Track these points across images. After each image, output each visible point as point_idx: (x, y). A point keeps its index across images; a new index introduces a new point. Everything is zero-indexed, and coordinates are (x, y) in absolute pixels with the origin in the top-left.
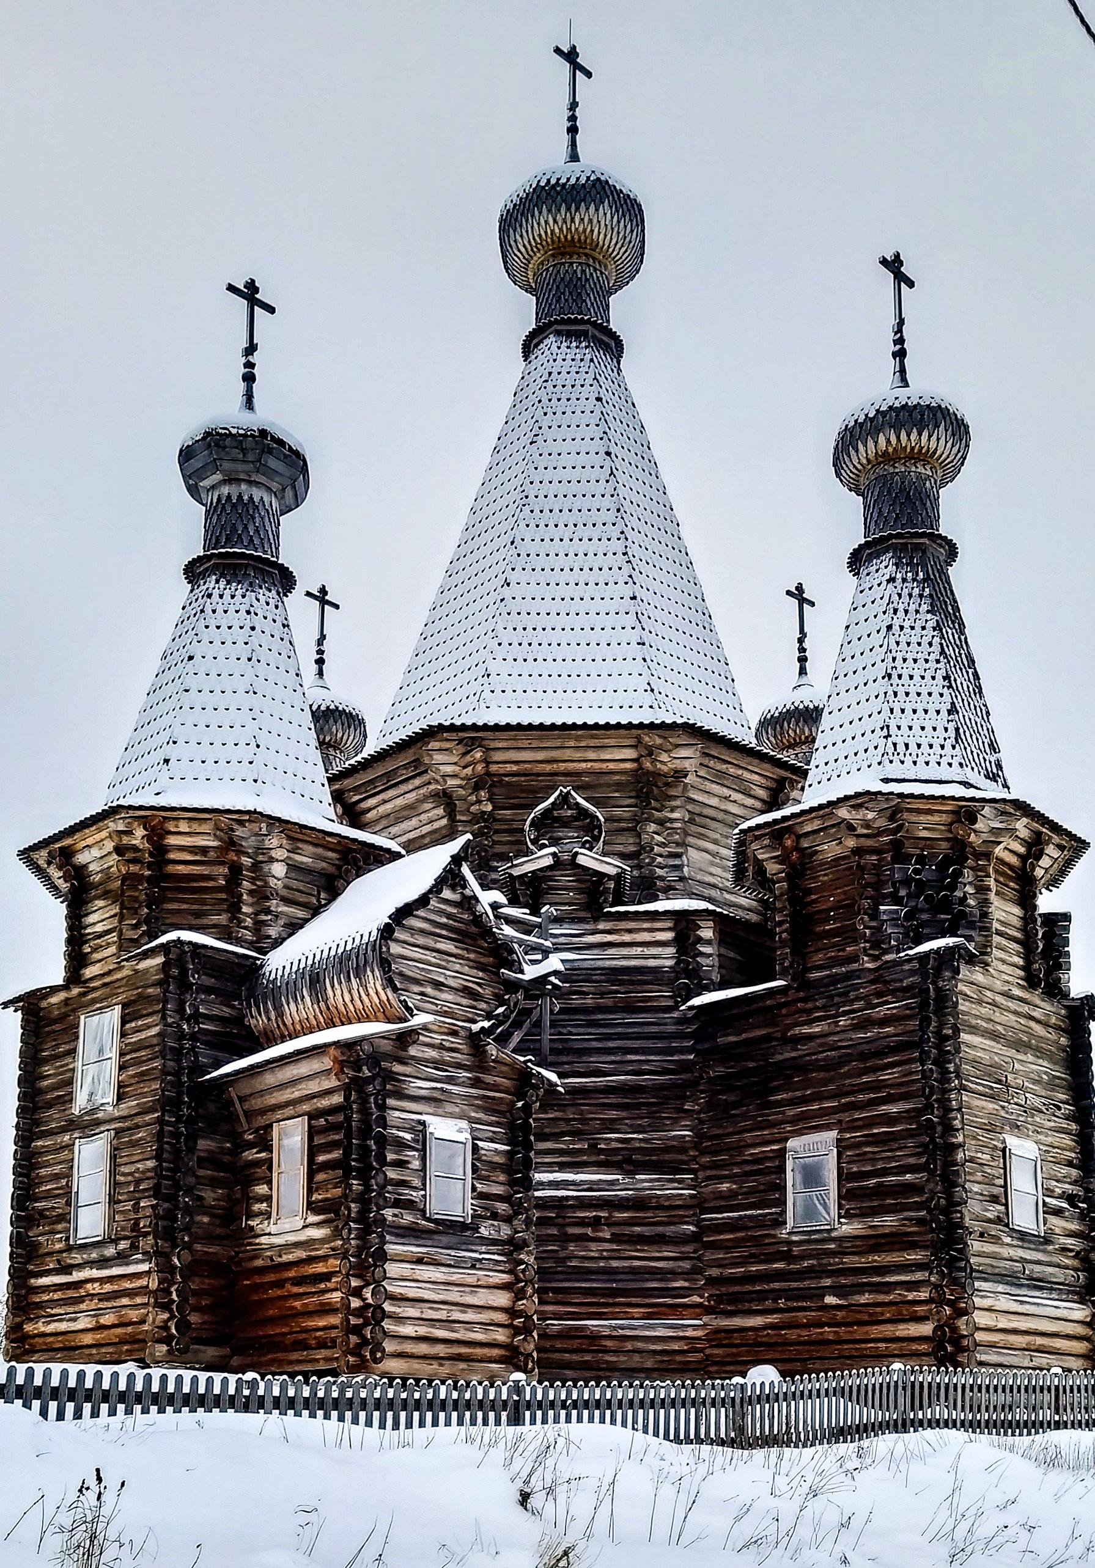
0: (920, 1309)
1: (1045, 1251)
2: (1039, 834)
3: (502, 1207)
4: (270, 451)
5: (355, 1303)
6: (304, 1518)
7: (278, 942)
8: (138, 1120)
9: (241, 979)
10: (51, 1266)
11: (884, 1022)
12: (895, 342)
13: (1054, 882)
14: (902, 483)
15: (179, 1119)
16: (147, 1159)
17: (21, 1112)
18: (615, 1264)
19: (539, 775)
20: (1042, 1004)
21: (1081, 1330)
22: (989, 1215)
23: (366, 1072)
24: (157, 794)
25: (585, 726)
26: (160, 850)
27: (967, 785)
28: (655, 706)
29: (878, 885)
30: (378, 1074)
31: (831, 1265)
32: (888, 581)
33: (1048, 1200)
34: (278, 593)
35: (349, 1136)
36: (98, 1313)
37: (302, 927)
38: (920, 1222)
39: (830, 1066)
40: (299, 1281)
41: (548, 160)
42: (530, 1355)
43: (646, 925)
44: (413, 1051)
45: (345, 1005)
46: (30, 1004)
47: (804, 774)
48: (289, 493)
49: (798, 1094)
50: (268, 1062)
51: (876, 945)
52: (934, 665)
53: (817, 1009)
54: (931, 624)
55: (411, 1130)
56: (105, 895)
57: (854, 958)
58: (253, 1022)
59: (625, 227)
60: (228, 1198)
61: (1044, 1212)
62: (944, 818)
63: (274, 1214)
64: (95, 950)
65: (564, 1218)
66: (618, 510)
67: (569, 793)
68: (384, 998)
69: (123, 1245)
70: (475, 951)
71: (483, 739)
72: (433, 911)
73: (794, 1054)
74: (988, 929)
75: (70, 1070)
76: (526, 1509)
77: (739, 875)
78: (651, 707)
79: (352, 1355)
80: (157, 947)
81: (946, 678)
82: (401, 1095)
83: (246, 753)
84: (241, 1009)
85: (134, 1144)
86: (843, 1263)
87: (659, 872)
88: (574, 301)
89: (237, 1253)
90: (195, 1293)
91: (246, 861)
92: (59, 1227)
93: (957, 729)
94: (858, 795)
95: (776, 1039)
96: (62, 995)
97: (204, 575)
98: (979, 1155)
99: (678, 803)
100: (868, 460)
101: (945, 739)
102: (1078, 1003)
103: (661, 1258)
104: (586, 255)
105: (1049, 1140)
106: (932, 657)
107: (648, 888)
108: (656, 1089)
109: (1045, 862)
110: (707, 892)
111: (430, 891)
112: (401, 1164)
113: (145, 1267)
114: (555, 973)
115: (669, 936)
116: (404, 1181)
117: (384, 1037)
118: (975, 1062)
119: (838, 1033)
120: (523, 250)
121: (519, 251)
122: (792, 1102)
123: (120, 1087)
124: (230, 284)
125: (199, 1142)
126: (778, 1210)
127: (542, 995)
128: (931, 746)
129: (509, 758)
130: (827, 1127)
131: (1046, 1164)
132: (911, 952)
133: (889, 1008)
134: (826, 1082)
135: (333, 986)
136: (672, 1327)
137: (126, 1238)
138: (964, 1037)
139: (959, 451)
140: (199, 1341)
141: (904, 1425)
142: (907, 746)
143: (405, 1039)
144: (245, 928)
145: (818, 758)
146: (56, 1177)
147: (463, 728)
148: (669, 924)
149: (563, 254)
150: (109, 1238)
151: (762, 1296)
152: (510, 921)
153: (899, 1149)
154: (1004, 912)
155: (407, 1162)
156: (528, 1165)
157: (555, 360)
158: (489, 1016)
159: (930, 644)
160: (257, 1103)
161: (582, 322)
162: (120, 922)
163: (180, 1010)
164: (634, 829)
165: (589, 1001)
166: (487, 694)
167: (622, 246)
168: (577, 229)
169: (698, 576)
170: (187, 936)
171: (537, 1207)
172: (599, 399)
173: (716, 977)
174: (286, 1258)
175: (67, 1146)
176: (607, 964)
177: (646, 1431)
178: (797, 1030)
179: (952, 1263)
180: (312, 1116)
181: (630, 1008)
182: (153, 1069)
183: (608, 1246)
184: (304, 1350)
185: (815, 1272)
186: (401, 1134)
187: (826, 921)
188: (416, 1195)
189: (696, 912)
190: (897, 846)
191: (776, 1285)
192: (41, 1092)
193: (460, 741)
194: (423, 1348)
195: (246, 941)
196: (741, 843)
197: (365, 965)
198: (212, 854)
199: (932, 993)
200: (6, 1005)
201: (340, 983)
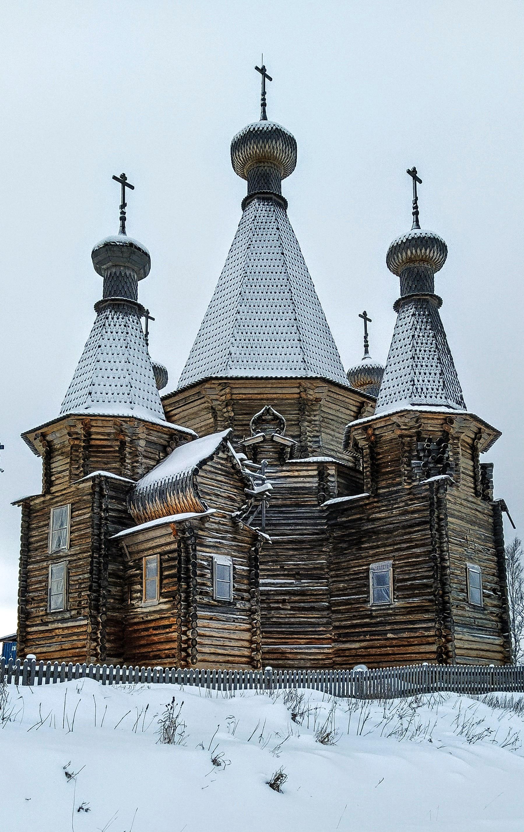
0: (430, 640)
1: (483, 614)
2: (480, 429)
3: (246, 595)
5: (184, 638)
6: (230, 721)
7: (142, 476)
8: (80, 556)
9: (127, 492)
10: (38, 622)
11: (413, 512)
12: (414, 208)
13: (485, 450)
14: (418, 271)
15: (100, 556)
16: (85, 574)
17: (22, 552)
18: (292, 620)
19: (255, 400)
20: (481, 504)
21: (499, 649)
22: (460, 598)
23: (187, 535)
24: (87, 408)
25: (276, 378)
26: (88, 434)
27: (448, 407)
28: (306, 368)
29: (410, 451)
30: (193, 536)
31: (390, 619)
32: (412, 315)
33: (485, 591)
34: (138, 317)
35: (180, 563)
36: (61, 643)
37: (152, 469)
38: (430, 601)
40: (155, 628)
41: (252, 119)
42: (259, 660)
43: (305, 468)
44: (207, 525)
45: (176, 504)
46: (26, 504)
47: (375, 401)
48: (142, 271)
49: (375, 544)
50: (142, 530)
51: (410, 478)
52: (432, 353)
53: (383, 506)
54: (431, 335)
55: (207, 560)
56: (62, 454)
57: (400, 484)
58: (131, 512)
59: (289, 151)
60: (122, 591)
61: (483, 596)
63: (144, 598)
64: (57, 479)
65: (269, 599)
66: (288, 280)
67: (269, 408)
68: (194, 501)
69: (73, 612)
70: (233, 480)
72: (215, 463)
73: (372, 526)
75: (46, 533)
76: (295, 721)
77: (346, 445)
78: (304, 369)
79: (182, 660)
80: (90, 478)
82: (202, 545)
83: (126, 390)
84: (126, 506)
85: (77, 567)
86: (395, 619)
87: (309, 444)
88: (266, 183)
89: (126, 616)
90: (109, 634)
91: (128, 439)
92: (42, 604)
93: (444, 382)
94: (401, 411)
95: (364, 519)
96: (42, 499)
97: (104, 309)
98: (456, 571)
100: (403, 261)
101: (439, 386)
102: (497, 503)
103: (313, 617)
104: (271, 163)
105: (485, 564)
106: (432, 350)
107: (304, 451)
109: (482, 440)
110: (332, 453)
111: (214, 454)
112: (202, 576)
113: (85, 622)
114: (268, 490)
115: (316, 473)
116: (204, 583)
117: (194, 518)
118: (453, 530)
119: (393, 517)
120: (242, 160)
121: (240, 160)
122: (372, 548)
123: (71, 541)
124: (114, 176)
125: (109, 567)
126: (366, 596)
127: (262, 500)
128: (433, 389)
129: (242, 392)
130: (388, 559)
132: (425, 481)
133: (417, 505)
134: (387, 539)
135: (170, 496)
136: (319, 648)
137: (75, 609)
138: (449, 519)
139: (443, 258)
140: (109, 655)
141: (428, 690)
142: (422, 389)
143: (203, 520)
144: (128, 469)
145: (382, 394)
146: (40, 582)
147: (221, 378)
148: (315, 468)
149: (260, 162)
150: (67, 609)
151: (359, 634)
152: (247, 466)
153: (421, 568)
154: (465, 463)
155: (206, 575)
156: (257, 575)
157: (257, 211)
158: (239, 509)
159: (431, 344)
160: (135, 549)
161: (270, 193)
162: (70, 466)
163: (100, 507)
164: (298, 425)
165: (280, 502)
166: (230, 363)
167: (287, 159)
168: (267, 151)
169: (323, 309)
170: (103, 473)
171: (261, 595)
172: (278, 229)
173: (336, 492)
174: (149, 618)
175: (45, 568)
176: (288, 485)
178: (374, 516)
180: (161, 554)
181: (298, 505)
182: (87, 533)
183: (289, 612)
184: (159, 659)
185: (383, 623)
186: (202, 562)
187: (387, 467)
188: (209, 589)
189: (327, 462)
190: (418, 434)
191: (365, 629)
192: (31, 543)
193: (220, 384)
194: (213, 658)
195: (128, 475)
196: (349, 432)
197: (186, 487)
198: (112, 436)
199: (435, 500)
200: (14, 504)
201: (174, 495)
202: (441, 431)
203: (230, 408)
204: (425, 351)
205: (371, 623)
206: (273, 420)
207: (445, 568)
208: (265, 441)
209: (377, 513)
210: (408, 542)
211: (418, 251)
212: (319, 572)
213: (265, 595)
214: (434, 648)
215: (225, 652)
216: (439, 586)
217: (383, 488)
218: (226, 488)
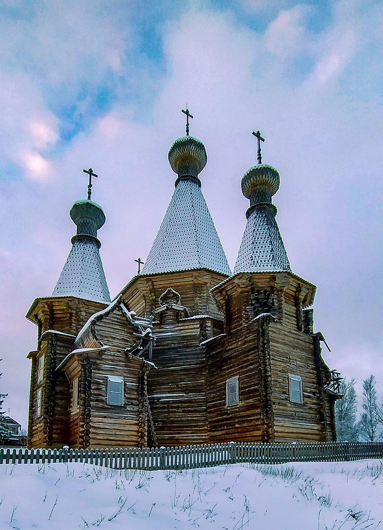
2: (299, 284)
3: (134, 402)
4: (90, 208)
11: (250, 341)
26: (52, 311)
33: (304, 393)
38: (259, 400)
39: (236, 357)
51: (247, 319)
53: (233, 341)
55: (103, 379)
62: (268, 280)
71: (151, 279)
74: (282, 312)
81: (271, 242)
93: (273, 256)
99: (205, 291)
108: (194, 369)
122: (228, 369)
131: (304, 383)
140: (57, 442)
143: (101, 353)
159: (266, 233)
170: (49, 331)
177: (101, 465)
179: (267, 412)
181: (188, 347)
194: (106, 442)
199: (261, 331)
202: (269, 287)
203: (153, 294)
204: (261, 238)
205: (228, 418)
206: (173, 296)
207: (267, 377)
208: (168, 309)
209: (230, 346)
210: (247, 362)
211: (258, 178)
212: (200, 388)
213: (166, 404)
214: (260, 433)
215: (117, 439)
216: (263, 389)
217: (234, 329)
218: (120, 333)
